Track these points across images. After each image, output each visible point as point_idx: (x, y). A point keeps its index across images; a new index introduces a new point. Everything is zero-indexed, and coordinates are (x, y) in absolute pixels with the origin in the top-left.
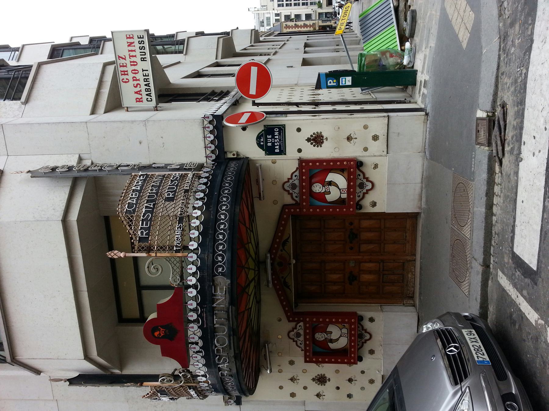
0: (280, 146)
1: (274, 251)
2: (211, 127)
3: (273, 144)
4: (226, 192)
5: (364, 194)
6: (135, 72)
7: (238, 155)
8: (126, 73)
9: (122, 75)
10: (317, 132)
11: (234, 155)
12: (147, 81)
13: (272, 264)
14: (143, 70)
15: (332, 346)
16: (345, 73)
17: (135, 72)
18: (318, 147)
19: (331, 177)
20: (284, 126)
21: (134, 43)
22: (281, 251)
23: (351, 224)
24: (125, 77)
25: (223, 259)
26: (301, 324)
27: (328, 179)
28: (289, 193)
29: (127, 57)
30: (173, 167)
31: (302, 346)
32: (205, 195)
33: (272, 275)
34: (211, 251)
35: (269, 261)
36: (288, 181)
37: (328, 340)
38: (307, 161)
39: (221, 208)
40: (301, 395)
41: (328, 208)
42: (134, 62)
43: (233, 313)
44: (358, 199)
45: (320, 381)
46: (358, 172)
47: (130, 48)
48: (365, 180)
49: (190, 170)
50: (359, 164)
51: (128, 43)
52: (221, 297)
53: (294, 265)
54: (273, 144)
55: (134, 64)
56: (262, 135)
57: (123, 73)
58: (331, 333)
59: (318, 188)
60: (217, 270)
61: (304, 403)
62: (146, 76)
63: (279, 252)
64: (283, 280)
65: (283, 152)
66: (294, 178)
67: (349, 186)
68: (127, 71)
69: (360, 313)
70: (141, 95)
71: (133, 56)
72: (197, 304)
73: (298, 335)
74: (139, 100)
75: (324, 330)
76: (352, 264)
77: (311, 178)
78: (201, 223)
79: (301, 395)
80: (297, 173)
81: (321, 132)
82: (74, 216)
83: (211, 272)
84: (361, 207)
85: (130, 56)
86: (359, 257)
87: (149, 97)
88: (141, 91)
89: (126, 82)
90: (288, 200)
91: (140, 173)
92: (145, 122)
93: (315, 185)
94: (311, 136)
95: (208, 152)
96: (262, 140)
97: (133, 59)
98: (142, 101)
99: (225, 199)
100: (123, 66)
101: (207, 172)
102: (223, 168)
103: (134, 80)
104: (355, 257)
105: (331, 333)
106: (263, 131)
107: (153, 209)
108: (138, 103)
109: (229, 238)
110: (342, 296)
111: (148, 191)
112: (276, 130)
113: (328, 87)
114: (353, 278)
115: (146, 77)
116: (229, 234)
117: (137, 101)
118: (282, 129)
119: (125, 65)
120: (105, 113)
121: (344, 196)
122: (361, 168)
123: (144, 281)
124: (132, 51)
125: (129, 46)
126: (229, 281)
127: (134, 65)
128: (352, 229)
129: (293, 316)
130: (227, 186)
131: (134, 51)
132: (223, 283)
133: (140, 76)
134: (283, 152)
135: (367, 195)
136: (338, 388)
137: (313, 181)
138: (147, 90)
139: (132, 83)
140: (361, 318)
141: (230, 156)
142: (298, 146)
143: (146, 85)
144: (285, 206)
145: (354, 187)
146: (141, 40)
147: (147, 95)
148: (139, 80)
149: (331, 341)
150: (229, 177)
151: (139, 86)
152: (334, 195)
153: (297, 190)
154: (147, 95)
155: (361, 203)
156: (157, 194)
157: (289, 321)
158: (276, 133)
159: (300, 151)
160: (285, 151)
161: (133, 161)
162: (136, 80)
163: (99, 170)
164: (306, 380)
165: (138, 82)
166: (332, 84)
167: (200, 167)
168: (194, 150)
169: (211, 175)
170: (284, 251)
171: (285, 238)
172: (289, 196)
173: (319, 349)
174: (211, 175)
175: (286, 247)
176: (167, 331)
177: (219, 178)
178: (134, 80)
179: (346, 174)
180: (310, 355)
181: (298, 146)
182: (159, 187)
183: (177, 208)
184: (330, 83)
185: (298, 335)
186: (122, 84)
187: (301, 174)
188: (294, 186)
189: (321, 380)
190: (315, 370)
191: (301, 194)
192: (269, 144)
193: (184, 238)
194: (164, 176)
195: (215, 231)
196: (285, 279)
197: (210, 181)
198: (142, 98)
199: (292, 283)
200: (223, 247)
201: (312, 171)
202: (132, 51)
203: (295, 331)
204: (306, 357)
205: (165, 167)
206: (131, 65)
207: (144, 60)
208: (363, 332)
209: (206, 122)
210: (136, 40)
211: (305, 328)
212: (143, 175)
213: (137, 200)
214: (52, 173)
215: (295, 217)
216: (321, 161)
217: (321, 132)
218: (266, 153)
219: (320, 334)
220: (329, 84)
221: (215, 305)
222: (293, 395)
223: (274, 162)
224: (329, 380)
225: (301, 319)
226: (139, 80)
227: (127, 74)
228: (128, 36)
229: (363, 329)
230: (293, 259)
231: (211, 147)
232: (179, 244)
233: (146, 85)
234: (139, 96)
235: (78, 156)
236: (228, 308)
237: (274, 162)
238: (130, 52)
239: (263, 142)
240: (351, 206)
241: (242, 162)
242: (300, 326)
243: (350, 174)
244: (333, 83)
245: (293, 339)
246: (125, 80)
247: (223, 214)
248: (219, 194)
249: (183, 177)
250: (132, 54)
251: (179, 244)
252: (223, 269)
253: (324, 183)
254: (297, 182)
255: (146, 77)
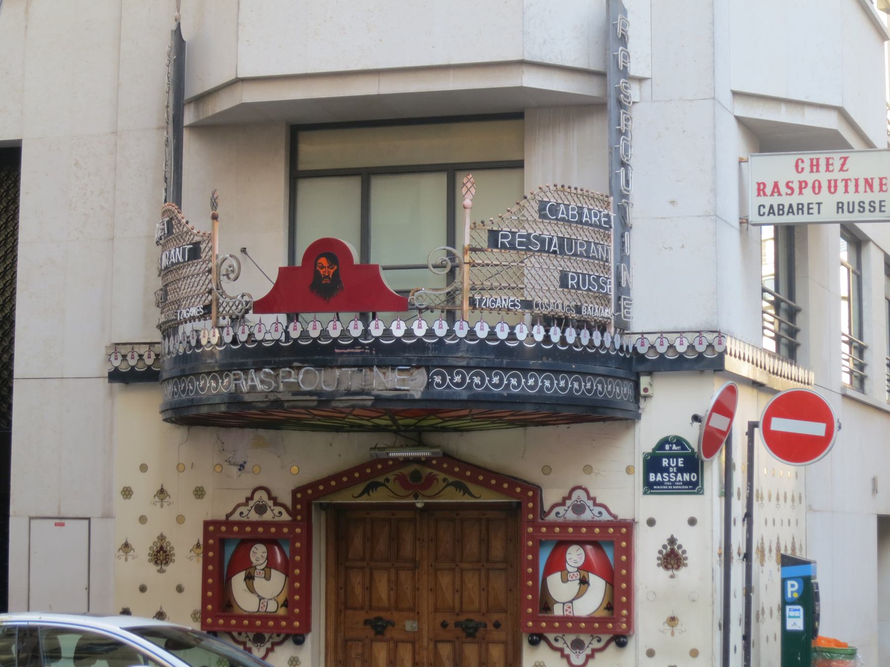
0: (661, 483)
1: (445, 466)
2: (700, 349)
3: (666, 470)
4: (576, 385)
5: (561, 650)
6: (817, 188)
7: (645, 397)
8: (815, 168)
9: (812, 160)
10: (686, 559)
11: (646, 390)
12: (798, 209)
13: (417, 460)
14: (819, 204)
15: (238, 581)
16: (812, 618)
17: (817, 188)
18: (658, 559)
19: (598, 585)
20: (700, 492)
21: (872, 190)
22: (445, 480)
23: (497, 625)
24: (807, 165)
25: (457, 385)
26: (286, 517)
27: (593, 579)
28: (565, 499)
29: (845, 175)
30: (624, 274)
31: (236, 517)
32: (571, 345)
33: (395, 459)
34: (472, 363)
35: (423, 453)
36: (589, 498)
37: (251, 570)
38: (629, 537)
39: (547, 378)
40: (127, 511)
41: (534, 576)
42: (836, 187)
43: (361, 403)
44: (551, 637)
45: (158, 552)
46: (605, 638)
47: (862, 183)
48: (588, 651)
49: (618, 308)
50: (620, 640)
51: (872, 179)
52: (386, 381)
53: (414, 505)
54: (666, 470)
55: (832, 187)
56: (684, 448)
57: (815, 162)
58: (268, 578)
59: (575, 556)
60: (437, 374)
61: (107, 516)
62: (809, 209)
63: (441, 476)
64: (381, 479)
65: (650, 487)
66: (597, 510)
67: (576, 620)
68: (818, 171)
69: (309, 638)
70: (772, 195)
71: (846, 186)
72: (377, 338)
73: (261, 509)
74: (761, 189)
75: (271, 564)
76: (410, 626)
77: (596, 544)
78: (521, 342)
79: (127, 511)
80: (606, 517)
81: (685, 565)
82: (532, 80)
83: (435, 363)
84: (534, 643)
85: (846, 181)
86: (425, 640)
87: (766, 210)
88: (780, 194)
89: (797, 166)
90: (550, 497)
91: (613, 215)
92: (715, 216)
93: (581, 551)
94: (680, 547)
95: (652, 338)
96: (674, 447)
97: (841, 186)
98: (759, 195)
99: (562, 384)
100: (828, 165)
101: (613, 342)
102: (621, 373)
103: (800, 183)
104: (425, 632)
105: (268, 578)
106: (693, 449)
107: (548, 252)
108: (756, 187)
109: (494, 395)
110: (341, 605)
111: (581, 235)
112: (694, 477)
113: (784, 581)
114: (379, 627)
115: (805, 209)
116: (500, 395)
117: (759, 184)
118: (695, 487)
119: (831, 168)
120: (739, 119)
121: (558, 611)
122: (613, 644)
123: (381, 188)
124: (857, 186)
125: (866, 180)
126: (418, 395)
127: (829, 187)
128: (485, 626)
129: (306, 498)
130: (585, 386)
131: (857, 191)
132: (413, 383)
133: (808, 197)
134: (650, 487)
135: (558, 654)
136: (143, 589)
137: (589, 547)
138: (781, 207)
139: (796, 178)
140: (299, 641)
141: (644, 381)
142: (660, 519)
143: (791, 206)
144: (537, 490)
145: (576, 630)
146: (877, 206)
147: (771, 207)
148: (801, 193)
149: (249, 578)
150: (603, 388)
151: (789, 191)
152: (560, 588)
153: (571, 516)
154: (771, 207)
155: (543, 646)
156: (575, 255)
157: (294, 492)
158: (686, 477)
159: (651, 522)
160: (651, 493)
161: (635, 191)
162: (801, 188)
163: (620, 130)
164: (161, 521)
165: (797, 191)
166: (790, 590)
167: (623, 327)
168: (655, 312)
169: (608, 352)
170: (445, 484)
171: (472, 488)
172: (559, 500)
173: (229, 551)
174: (608, 352)
175: (451, 489)
176: (329, 282)
177: (600, 369)
178: (800, 183)
179: (604, 613)
180: (221, 532)
181: (660, 519)
182: (588, 257)
183: (548, 294)
184: (793, 586)
185: (261, 509)
186: (796, 157)
187: (604, 526)
188: (579, 508)
189: (161, 555)
190: (186, 541)
191: (564, 526)
192: (665, 462)
193: (495, 313)
194: (607, 261)
195: (506, 369)
196: (384, 485)
197: (597, 352)
198: (765, 194)
199: (379, 497)
200: (477, 386)
201: (610, 545)
202: (857, 186)
203: (270, 503)
204: (216, 523)
205: (623, 258)
206: (830, 181)
207: (838, 208)
208: (269, 645)
209: (710, 337)
210: (876, 196)
211: (279, 525)
212: (608, 222)
213: (563, 219)
214: (613, 35)
215: (513, 511)
216: (629, 565)
217: (685, 565)
218: (648, 454)
219: (265, 555)
220: (789, 583)
221: (375, 369)
222: (127, 493)
223: (629, 470)
224: (161, 571)
225: (299, 518)
226: (801, 193)
227: (812, 171)
228: (884, 181)
229: (274, 644)
230: (426, 504)
231: (662, 345)
232: (485, 304)
233: (791, 206)
234: (768, 190)
235: (646, 76)
236: (368, 393)
237: (629, 470)
238: (854, 182)
239: (671, 449)
240: (537, 621)
241: (632, 407)
242: (280, 513)
243: (602, 621)
244: (792, 592)
245: (251, 498)
246: (801, 165)
247: (536, 382)
248: (570, 373)
249: (605, 297)
250: (851, 185)
251: (485, 304)
252: (438, 385)
253: (587, 567)
254: (587, 516)
255: (805, 209)
